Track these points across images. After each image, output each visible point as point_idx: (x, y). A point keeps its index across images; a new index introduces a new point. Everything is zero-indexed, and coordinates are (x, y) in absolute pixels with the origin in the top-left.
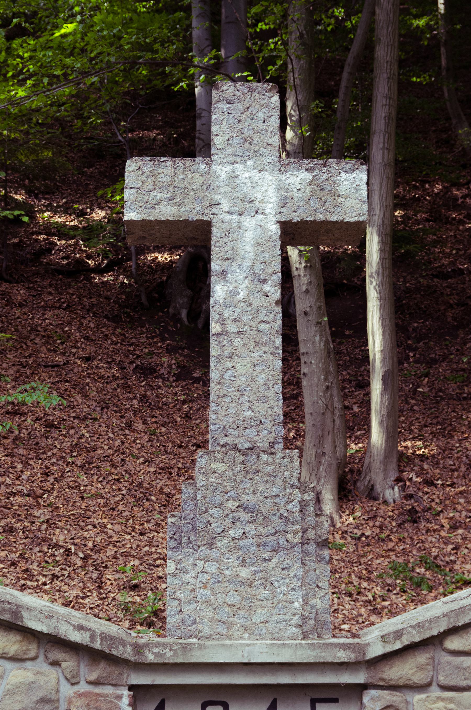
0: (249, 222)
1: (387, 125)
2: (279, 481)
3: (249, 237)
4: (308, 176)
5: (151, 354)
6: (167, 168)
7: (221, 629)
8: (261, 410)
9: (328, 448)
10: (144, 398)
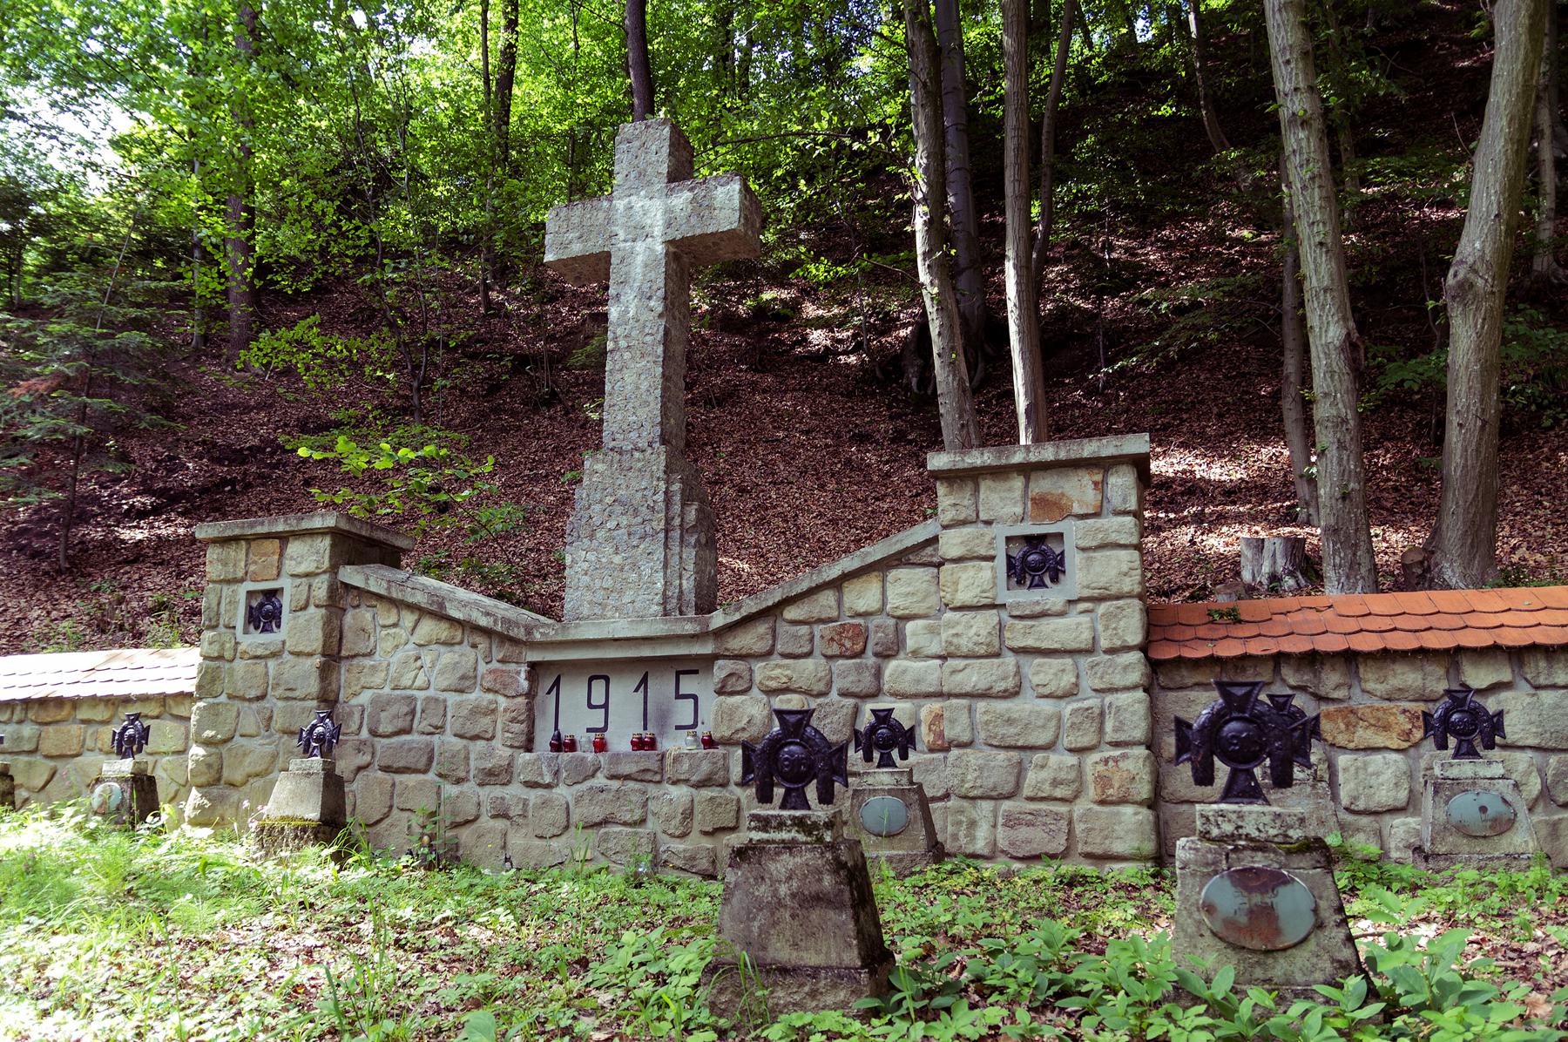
0: (640, 246)
1: (1016, 156)
2: (648, 475)
3: (640, 259)
4: (687, 195)
7: (597, 610)
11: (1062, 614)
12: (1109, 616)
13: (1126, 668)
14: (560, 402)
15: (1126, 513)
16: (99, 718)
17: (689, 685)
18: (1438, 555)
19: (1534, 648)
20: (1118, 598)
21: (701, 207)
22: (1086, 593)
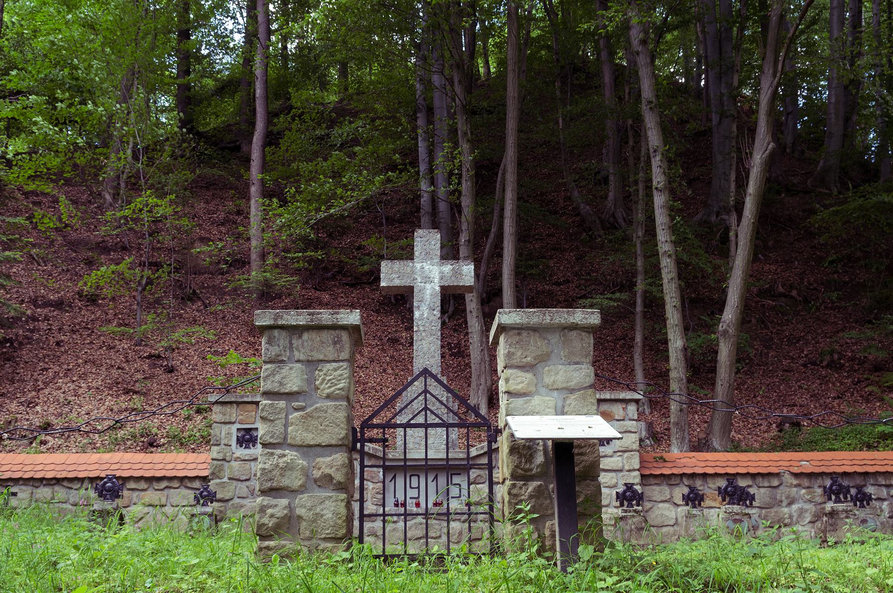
0: (428, 286)
3: (428, 292)
5: (396, 331)
6: (397, 265)
8: (432, 361)
9: (483, 381)
10: (392, 357)
11: (611, 456)
12: (628, 458)
13: (634, 477)
14: (199, 298)
15: (634, 420)
16: (142, 488)
17: (456, 479)
18: (711, 435)
19: (759, 474)
20: (631, 451)
21: (456, 273)
22: (621, 449)
